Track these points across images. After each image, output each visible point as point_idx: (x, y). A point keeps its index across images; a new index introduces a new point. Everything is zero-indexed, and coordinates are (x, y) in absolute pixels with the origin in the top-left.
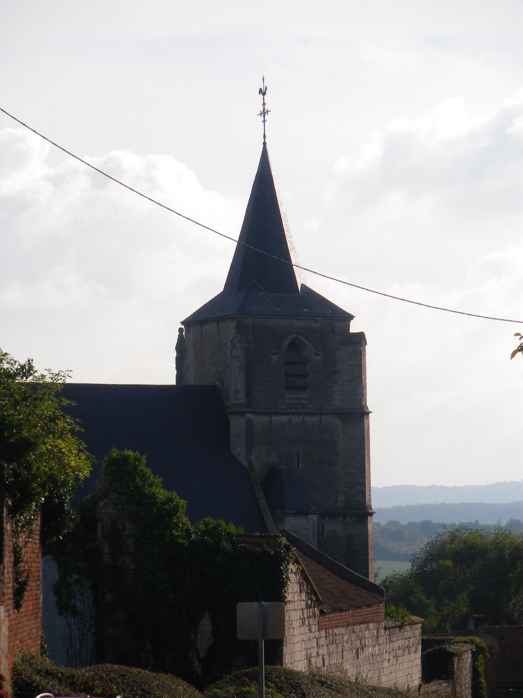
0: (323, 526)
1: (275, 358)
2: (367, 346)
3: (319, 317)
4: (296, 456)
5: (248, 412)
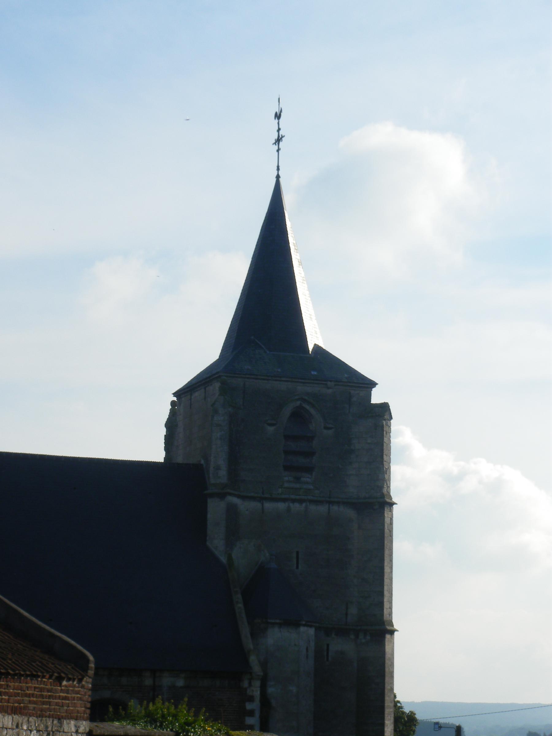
0: (328, 645)
1: (271, 429)
2: (392, 421)
3: (331, 381)
4: (295, 555)
5: (230, 494)
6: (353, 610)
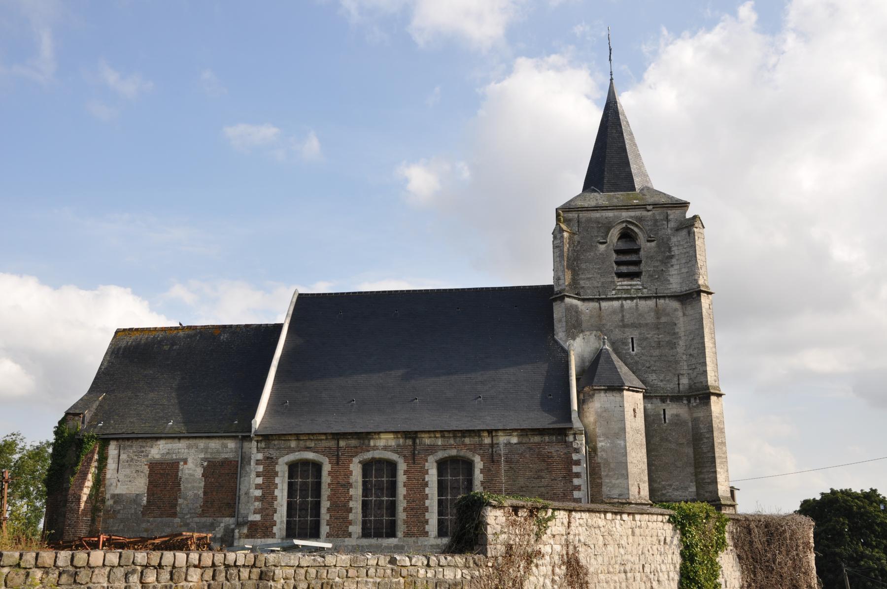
4: (630, 340)
5: (569, 297)
6: (685, 381)
